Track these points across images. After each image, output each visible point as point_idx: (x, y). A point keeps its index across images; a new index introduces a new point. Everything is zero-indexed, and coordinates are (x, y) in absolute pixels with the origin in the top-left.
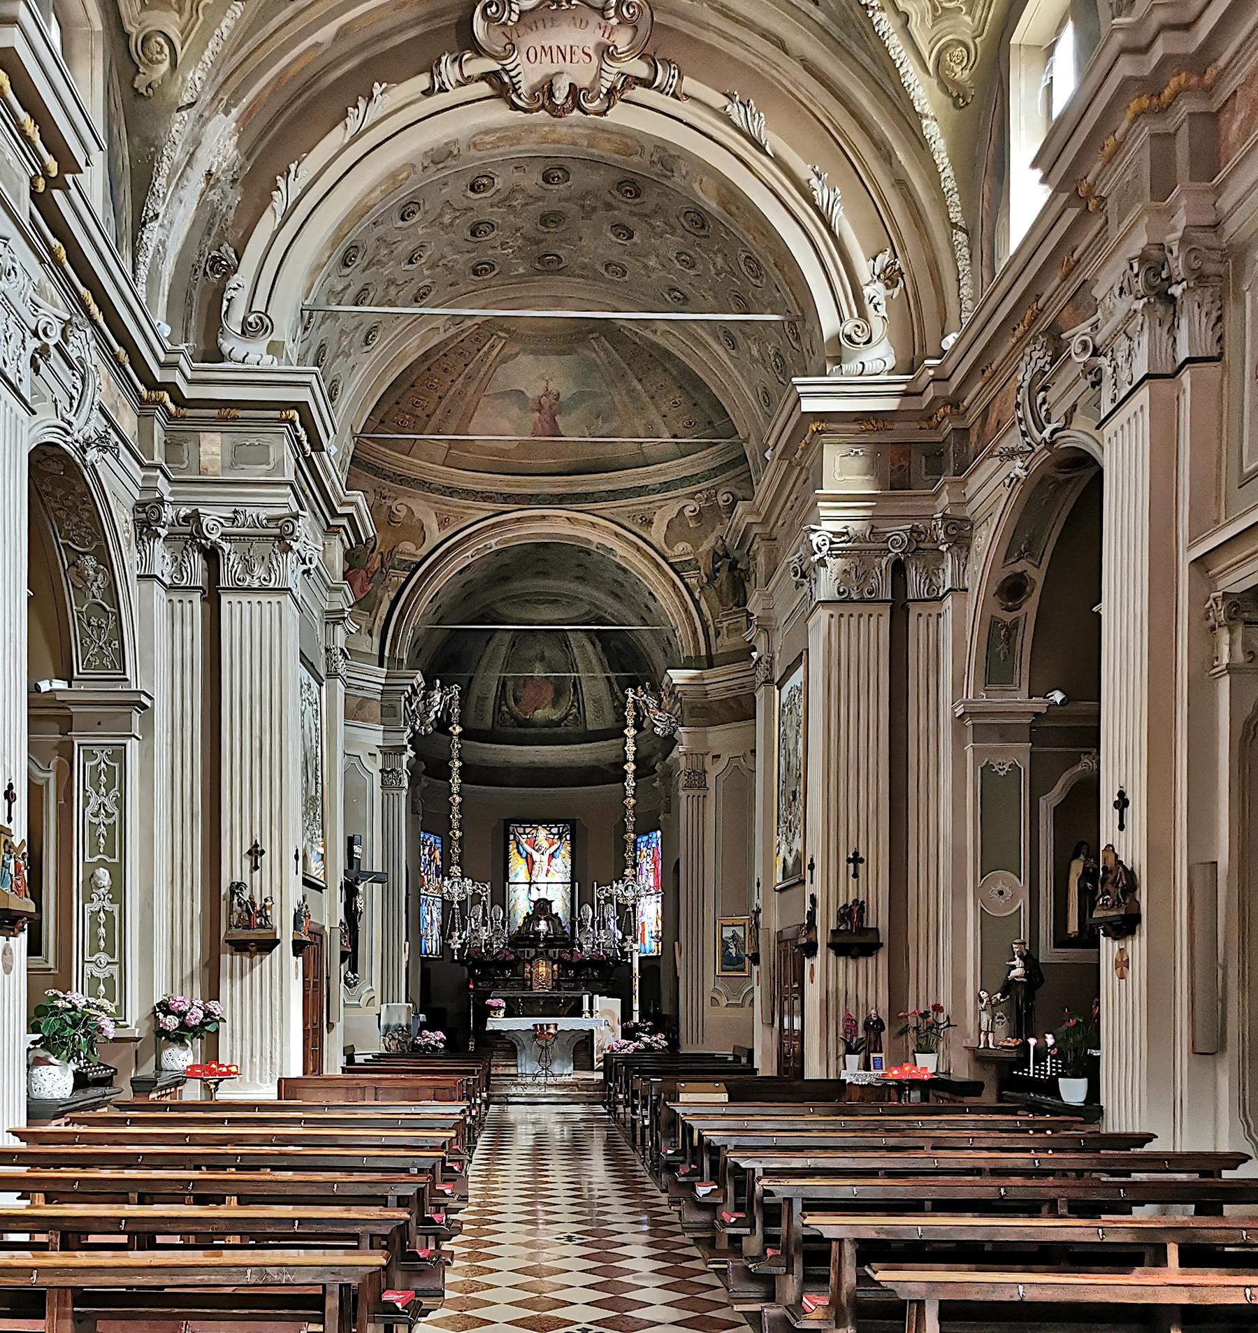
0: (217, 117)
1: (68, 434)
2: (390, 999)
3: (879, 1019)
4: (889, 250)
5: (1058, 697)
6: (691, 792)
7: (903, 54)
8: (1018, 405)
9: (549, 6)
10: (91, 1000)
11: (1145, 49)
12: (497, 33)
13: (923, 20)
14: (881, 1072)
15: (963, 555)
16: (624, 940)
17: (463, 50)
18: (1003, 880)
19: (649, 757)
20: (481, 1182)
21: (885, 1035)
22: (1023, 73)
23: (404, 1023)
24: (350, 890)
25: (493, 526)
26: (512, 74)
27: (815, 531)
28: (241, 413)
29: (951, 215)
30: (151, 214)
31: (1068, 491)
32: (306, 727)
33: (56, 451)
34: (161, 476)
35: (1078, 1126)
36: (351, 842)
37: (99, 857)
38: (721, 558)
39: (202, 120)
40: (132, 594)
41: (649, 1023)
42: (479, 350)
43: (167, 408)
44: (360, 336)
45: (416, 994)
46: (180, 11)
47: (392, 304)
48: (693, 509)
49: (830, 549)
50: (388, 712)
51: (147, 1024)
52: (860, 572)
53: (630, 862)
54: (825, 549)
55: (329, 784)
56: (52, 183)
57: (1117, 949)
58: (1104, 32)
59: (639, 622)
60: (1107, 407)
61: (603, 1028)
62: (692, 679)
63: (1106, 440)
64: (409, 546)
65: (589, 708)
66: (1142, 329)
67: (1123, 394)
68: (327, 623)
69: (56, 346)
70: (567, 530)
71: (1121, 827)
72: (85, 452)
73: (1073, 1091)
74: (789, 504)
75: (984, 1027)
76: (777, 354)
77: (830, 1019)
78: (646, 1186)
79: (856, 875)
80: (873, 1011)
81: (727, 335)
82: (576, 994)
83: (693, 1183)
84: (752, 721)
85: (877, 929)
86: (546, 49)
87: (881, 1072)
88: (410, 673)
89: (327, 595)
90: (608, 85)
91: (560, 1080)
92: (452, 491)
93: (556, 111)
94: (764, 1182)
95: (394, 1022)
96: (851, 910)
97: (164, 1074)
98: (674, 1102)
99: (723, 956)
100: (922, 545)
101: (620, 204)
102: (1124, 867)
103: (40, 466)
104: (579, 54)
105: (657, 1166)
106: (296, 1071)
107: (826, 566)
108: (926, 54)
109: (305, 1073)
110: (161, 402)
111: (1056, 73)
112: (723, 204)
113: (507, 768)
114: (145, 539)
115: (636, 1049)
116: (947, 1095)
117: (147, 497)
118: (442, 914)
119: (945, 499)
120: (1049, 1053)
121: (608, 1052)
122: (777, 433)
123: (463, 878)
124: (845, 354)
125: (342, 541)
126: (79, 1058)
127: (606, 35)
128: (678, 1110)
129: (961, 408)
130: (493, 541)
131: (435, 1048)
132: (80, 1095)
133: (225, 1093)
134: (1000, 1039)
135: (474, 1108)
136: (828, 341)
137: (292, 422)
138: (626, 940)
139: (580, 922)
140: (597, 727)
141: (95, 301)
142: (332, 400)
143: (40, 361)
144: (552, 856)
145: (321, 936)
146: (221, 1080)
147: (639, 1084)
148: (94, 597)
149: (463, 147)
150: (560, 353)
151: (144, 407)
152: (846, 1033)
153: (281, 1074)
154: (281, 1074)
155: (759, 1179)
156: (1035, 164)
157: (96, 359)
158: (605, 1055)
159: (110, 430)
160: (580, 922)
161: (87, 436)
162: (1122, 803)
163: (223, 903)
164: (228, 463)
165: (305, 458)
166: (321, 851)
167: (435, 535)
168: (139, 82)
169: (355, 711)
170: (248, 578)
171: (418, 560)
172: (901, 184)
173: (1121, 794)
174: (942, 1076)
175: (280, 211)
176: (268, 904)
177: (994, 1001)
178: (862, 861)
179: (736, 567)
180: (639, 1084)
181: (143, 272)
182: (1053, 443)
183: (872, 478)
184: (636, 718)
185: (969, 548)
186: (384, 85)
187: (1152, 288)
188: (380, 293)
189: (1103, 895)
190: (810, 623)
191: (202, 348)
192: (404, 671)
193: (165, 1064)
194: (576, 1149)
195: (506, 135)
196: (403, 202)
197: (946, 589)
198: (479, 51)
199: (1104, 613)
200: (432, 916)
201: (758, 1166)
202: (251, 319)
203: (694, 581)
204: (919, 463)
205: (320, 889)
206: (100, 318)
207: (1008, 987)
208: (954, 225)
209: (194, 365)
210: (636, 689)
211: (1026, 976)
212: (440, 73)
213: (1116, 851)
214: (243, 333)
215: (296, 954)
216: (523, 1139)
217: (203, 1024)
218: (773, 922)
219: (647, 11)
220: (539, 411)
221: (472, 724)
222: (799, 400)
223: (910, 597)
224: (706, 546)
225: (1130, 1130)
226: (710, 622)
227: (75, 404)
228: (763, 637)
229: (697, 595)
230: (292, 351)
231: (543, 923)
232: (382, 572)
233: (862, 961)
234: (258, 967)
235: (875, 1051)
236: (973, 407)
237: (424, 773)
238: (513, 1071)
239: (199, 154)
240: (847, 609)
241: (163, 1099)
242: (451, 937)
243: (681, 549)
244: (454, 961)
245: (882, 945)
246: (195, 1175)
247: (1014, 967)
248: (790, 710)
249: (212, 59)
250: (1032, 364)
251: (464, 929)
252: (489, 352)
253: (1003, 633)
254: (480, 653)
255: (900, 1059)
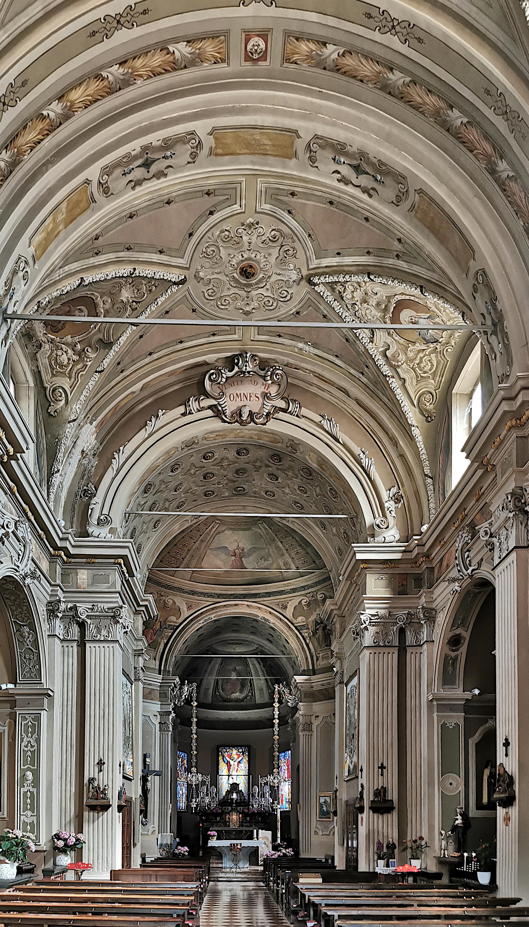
0: (87, 425)
1: (17, 571)
2: (163, 832)
3: (393, 843)
4: (396, 486)
5: (477, 692)
6: (305, 733)
7: (403, 398)
8: (456, 558)
9: (239, 375)
10: (24, 834)
11: (514, 399)
12: (215, 387)
13: (412, 382)
14: (394, 868)
15: (432, 625)
16: (273, 803)
17: (200, 395)
18: (452, 778)
19: (285, 716)
20: (206, 919)
21: (396, 851)
22: (458, 406)
23: (169, 843)
24: (144, 780)
25: (213, 609)
26: (223, 406)
27: (363, 614)
28: (97, 561)
29: (425, 471)
30: (56, 470)
31: (479, 597)
32: (125, 704)
33: (11, 579)
34: (60, 590)
35: (487, 895)
36: (145, 756)
37: (27, 766)
38: (319, 624)
39: (80, 427)
40: (45, 643)
41: (285, 843)
42: (207, 529)
43: (63, 559)
44: (152, 525)
45: (175, 830)
46: (70, 378)
47: (166, 510)
48: (305, 601)
49: (370, 622)
50: (163, 696)
51: (49, 844)
52: (384, 633)
53: (276, 766)
54: (367, 622)
55: (135, 730)
56: (10, 458)
57: (505, 812)
58: (495, 390)
59: (280, 653)
60: (497, 561)
61: (263, 846)
62: (306, 680)
63: (497, 576)
64: (173, 618)
65: (257, 694)
66: (512, 525)
67: (504, 555)
68: (135, 655)
69: (13, 532)
70: (248, 611)
71: (507, 755)
72: (25, 579)
73: (484, 878)
74: (350, 601)
75: (443, 847)
76: (345, 532)
77: (371, 844)
78: (283, 921)
79: (382, 775)
80: (391, 840)
81: (322, 524)
82: (251, 829)
83: (306, 920)
84: (333, 700)
85: (392, 800)
86: (238, 394)
87: (394, 868)
88: (174, 677)
89: (135, 642)
90: (267, 411)
91: (242, 870)
92: (193, 593)
93: (242, 423)
94: (338, 922)
95: (164, 843)
96: (380, 791)
97: (57, 868)
98: (296, 882)
99: (320, 811)
100: (413, 621)
101: (272, 465)
102: (508, 774)
103: (4, 586)
104: (253, 397)
105: (289, 912)
106: (118, 866)
107: (368, 630)
108: (413, 398)
109: (123, 867)
110: (60, 556)
111: (473, 407)
112: (320, 465)
113: (218, 721)
114: (52, 618)
115: (279, 856)
116: (425, 879)
117: (53, 599)
118: (187, 790)
119: (423, 599)
120: (473, 860)
121: (265, 857)
122: (345, 568)
123: (197, 773)
124: (376, 534)
125: (142, 617)
126: (19, 860)
127: (266, 388)
128: (299, 887)
129: (430, 558)
130: (213, 616)
131: (184, 855)
132: (20, 877)
133: (86, 877)
134: (451, 853)
135: (202, 884)
136: (368, 527)
137: (120, 564)
138: (274, 803)
139: (252, 794)
140: (259, 702)
141: (30, 510)
142: (138, 553)
143: (5, 539)
144: (239, 762)
145: (131, 802)
146: (84, 871)
147: (280, 873)
148: (28, 645)
149: (200, 440)
150: (243, 530)
151: (52, 558)
152: (378, 849)
153: (112, 868)
154: (112, 868)
155: (336, 921)
156: (463, 451)
157: (30, 537)
158: (264, 859)
159: (37, 570)
160: (252, 794)
161: (26, 572)
162: (507, 744)
163: (85, 788)
164: (90, 583)
165: (126, 580)
166: (131, 760)
167: (185, 613)
168: (51, 410)
169: (147, 696)
170: (99, 635)
171: (178, 625)
172: (402, 456)
173: (506, 740)
174: (423, 870)
175: (115, 469)
176: (106, 788)
177: (448, 835)
178: (385, 768)
179: (326, 628)
180: (280, 873)
181: (52, 496)
182: (472, 576)
183: (390, 589)
184: (279, 698)
185: (434, 623)
186: (164, 411)
187: (517, 507)
188: (161, 505)
189: (498, 787)
190: (361, 656)
191: (79, 531)
192: (171, 677)
193: (58, 863)
194: (250, 902)
195: (219, 434)
196: (172, 464)
197: (424, 641)
198: (208, 396)
199: (497, 655)
200: (182, 791)
201: (336, 914)
202: (102, 518)
203: (306, 634)
204: (412, 583)
205: (130, 780)
206: (32, 519)
207: (455, 828)
208: (426, 475)
209: (75, 539)
210: (279, 685)
211: (463, 823)
212: (190, 406)
213: (504, 766)
214: (98, 524)
215: (119, 812)
216: (225, 898)
217: (75, 844)
218: (343, 796)
219: (285, 377)
220: (235, 556)
221: (202, 700)
222: (355, 553)
223: (407, 644)
224: (312, 618)
225: (510, 897)
226: (314, 654)
227: (21, 558)
228: (338, 662)
229: (308, 641)
230: (120, 532)
231: (235, 794)
232: (160, 630)
233: (385, 816)
234: (101, 818)
235: (392, 858)
236: (435, 559)
237: (179, 723)
238: (220, 865)
239: (78, 442)
240: (378, 650)
241: (57, 879)
242: (191, 802)
243: (300, 620)
244: (192, 813)
245: (394, 808)
246: (72, 917)
247: (457, 819)
248: (351, 697)
249: (85, 399)
250: (463, 539)
251: (198, 797)
252: (212, 529)
253: (450, 662)
254: (205, 669)
255: (403, 862)
